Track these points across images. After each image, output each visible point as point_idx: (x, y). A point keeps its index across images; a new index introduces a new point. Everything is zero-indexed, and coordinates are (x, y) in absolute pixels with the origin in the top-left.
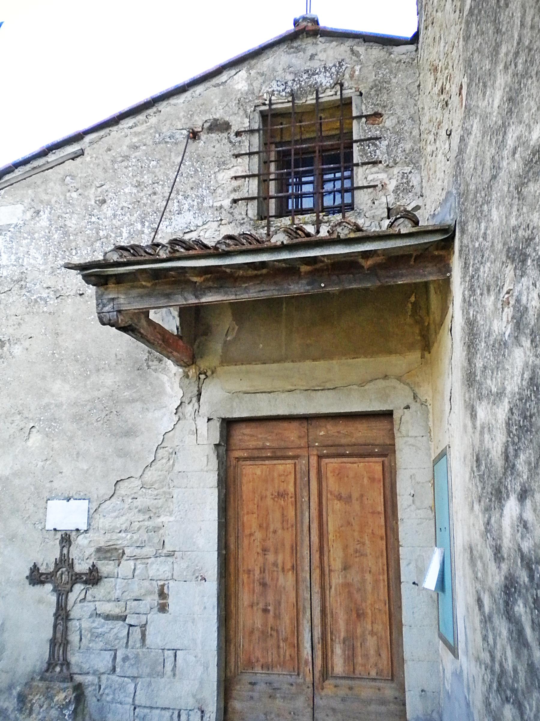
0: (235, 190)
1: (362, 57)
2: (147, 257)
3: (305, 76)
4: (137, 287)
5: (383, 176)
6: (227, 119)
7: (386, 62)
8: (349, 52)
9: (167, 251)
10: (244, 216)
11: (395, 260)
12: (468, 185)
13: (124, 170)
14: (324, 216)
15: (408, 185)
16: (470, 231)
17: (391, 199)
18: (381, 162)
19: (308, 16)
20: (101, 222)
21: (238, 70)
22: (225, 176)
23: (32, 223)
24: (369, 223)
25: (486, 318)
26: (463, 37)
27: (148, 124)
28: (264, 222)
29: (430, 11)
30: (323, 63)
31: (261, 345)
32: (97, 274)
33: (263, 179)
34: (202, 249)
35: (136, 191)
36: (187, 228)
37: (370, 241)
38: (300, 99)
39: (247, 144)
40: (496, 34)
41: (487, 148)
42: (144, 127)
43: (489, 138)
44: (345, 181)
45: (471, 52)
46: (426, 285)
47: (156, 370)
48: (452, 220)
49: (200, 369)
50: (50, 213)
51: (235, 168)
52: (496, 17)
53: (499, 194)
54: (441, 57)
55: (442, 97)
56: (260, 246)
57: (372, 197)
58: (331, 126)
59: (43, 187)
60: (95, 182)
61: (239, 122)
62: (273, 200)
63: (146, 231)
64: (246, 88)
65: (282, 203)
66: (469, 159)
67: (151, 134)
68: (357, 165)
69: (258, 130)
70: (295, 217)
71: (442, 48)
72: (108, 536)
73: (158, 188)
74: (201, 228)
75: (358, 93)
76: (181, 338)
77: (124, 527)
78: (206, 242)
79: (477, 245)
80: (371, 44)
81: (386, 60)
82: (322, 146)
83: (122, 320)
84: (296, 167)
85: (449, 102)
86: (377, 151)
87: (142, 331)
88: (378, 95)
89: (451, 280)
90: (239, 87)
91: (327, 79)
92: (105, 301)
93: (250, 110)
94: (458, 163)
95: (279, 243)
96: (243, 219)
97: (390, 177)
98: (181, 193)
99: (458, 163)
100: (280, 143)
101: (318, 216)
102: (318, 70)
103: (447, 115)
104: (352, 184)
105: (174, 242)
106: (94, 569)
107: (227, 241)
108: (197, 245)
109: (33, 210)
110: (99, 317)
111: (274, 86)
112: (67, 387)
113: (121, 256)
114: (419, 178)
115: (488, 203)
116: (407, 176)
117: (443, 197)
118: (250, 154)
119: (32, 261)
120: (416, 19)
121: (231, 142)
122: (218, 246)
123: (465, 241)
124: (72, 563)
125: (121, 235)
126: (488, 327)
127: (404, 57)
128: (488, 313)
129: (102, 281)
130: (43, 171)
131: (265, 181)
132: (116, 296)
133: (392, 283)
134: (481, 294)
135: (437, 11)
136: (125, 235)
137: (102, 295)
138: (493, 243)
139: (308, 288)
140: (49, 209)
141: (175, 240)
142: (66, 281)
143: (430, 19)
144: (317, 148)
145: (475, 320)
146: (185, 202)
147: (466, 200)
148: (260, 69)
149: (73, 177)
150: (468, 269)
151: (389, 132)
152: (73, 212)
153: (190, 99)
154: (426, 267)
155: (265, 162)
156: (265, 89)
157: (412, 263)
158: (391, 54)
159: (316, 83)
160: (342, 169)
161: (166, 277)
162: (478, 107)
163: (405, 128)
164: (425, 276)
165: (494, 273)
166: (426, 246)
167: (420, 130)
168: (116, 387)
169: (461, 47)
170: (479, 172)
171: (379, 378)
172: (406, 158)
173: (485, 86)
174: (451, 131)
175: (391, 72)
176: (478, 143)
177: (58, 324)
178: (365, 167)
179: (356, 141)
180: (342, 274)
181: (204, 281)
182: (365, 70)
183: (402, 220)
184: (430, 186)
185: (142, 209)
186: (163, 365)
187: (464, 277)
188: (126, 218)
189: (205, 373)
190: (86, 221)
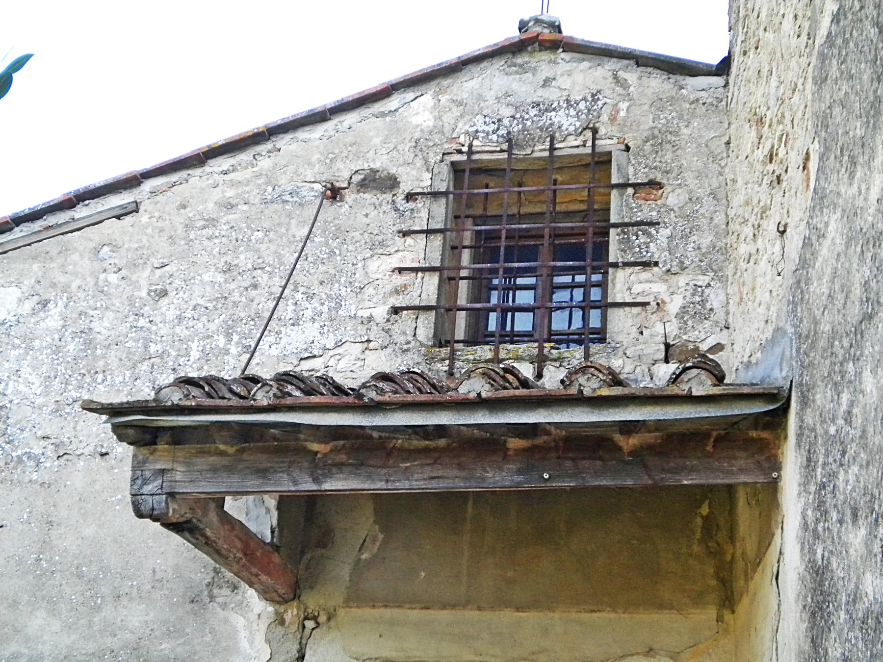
0: (397, 292)
1: (632, 89)
2: (235, 401)
3: (533, 112)
4: (209, 453)
5: (659, 288)
6: (393, 171)
7: (672, 100)
8: (611, 80)
9: (271, 394)
10: (410, 338)
11: (680, 441)
12: (816, 323)
13: (206, 242)
14: (552, 348)
15: (704, 307)
16: (818, 402)
17: (673, 328)
18: (656, 264)
19: (544, 17)
20: (154, 328)
21: (419, 94)
22: (380, 267)
23: (33, 320)
24: (632, 367)
25: (849, 566)
26: (814, 78)
27: (254, 169)
28: (445, 351)
29: (753, 28)
30: (565, 93)
31: (423, 574)
32: (141, 426)
33: (448, 277)
34: (334, 394)
35: (222, 280)
36: (306, 350)
37: (636, 404)
38: (521, 147)
39: (424, 214)
40: (875, 84)
41: (855, 265)
42: (248, 173)
43: (859, 249)
44: (593, 290)
45: (828, 104)
46: (730, 489)
47: (224, 606)
48: (785, 378)
49: (306, 608)
50: (66, 306)
51: (400, 253)
52: (876, 56)
53: (877, 348)
54: (772, 103)
55: (771, 168)
56: (437, 397)
57: (638, 321)
58: (573, 195)
59: (60, 260)
60: (152, 260)
61: (414, 177)
62: (462, 315)
63: (233, 350)
64: (431, 124)
65: (478, 317)
66: (820, 279)
67: (259, 185)
68: (615, 265)
69: (446, 194)
70: (501, 346)
71: (773, 91)
73: (262, 278)
74: (331, 353)
75: (623, 147)
76: (277, 548)
78: (338, 379)
79: (832, 430)
80: (649, 69)
81: (673, 97)
82: (555, 228)
83: (174, 510)
84: (506, 261)
85: (784, 177)
86: (651, 244)
87: (208, 532)
88: (657, 152)
89: (781, 484)
90: (415, 120)
91: (571, 120)
92: (147, 474)
93: (434, 158)
94: (799, 282)
95: (473, 395)
96: (408, 343)
97: (671, 290)
98: (302, 289)
99: (799, 282)
100: (481, 217)
101: (541, 348)
102: (555, 104)
103: (778, 198)
104: (605, 294)
105: (284, 378)
107: (380, 385)
108: (325, 385)
109: (36, 299)
110: (133, 503)
111: (479, 124)
112: (56, 625)
113: (187, 396)
114: (722, 297)
115: (856, 359)
116: (703, 292)
117: (768, 334)
118: (428, 232)
119: (22, 388)
120: (726, 37)
121: (396, 210)
122: (363, 391)
123: (809, 420)
125: (188, 354)
126: (853, 585)
127: (703, 94)
128: (853, 558)
129: (148, 437)
130: (62, 234)
131: (450, 279)
132: (167, 466)
133: (671, 482)
134: (841, 522)
135: (765, 30)
136: (195, 354)
137: (145, 462)
138: (864, 431)
139: (518, 478)
140: (65, 300)
141: (286, 374)
142: (78, 428)
143: (753, 41)
144: (547, 231)
145: (827, 567)
146: (309, 306)
147: (813, 346)
148: (457, 95)
149: (115, 248)
150: (814, 470)
151: (673, 215)
152: (107, 308)
153: (332, 133)
154: (734, 458)
155: (454, 248)
156: (462, 127)
157: (709, 448)
158: (681, 88)
159: (552, 124)
160: (589, 270)
161: (262, 438)
162: (839, 194)
163: (702, 211)
164: (733, 473)
165: (865, 487)
166: (735, 420)
167: (727, 216)
168: (148, 631)
169: (808, 92)
170: (839, 304)
171: (637, 653)
172: (701, 261)
173: (853, 161)
174: (786, 226)
175: (681, 117)
176: (839, 255)
177: (54, 506)
178: (629, 270)
179: (616, 226)
180: (584, 459)
181: (331, 451)
182: (636, 111)
183: (695, 371)
184: (743, 313)
185: (231, 312)
186: (239, 597)
187: (805, 485)
188: (200, 325)
189: (315, 618)
190: (128, 325)
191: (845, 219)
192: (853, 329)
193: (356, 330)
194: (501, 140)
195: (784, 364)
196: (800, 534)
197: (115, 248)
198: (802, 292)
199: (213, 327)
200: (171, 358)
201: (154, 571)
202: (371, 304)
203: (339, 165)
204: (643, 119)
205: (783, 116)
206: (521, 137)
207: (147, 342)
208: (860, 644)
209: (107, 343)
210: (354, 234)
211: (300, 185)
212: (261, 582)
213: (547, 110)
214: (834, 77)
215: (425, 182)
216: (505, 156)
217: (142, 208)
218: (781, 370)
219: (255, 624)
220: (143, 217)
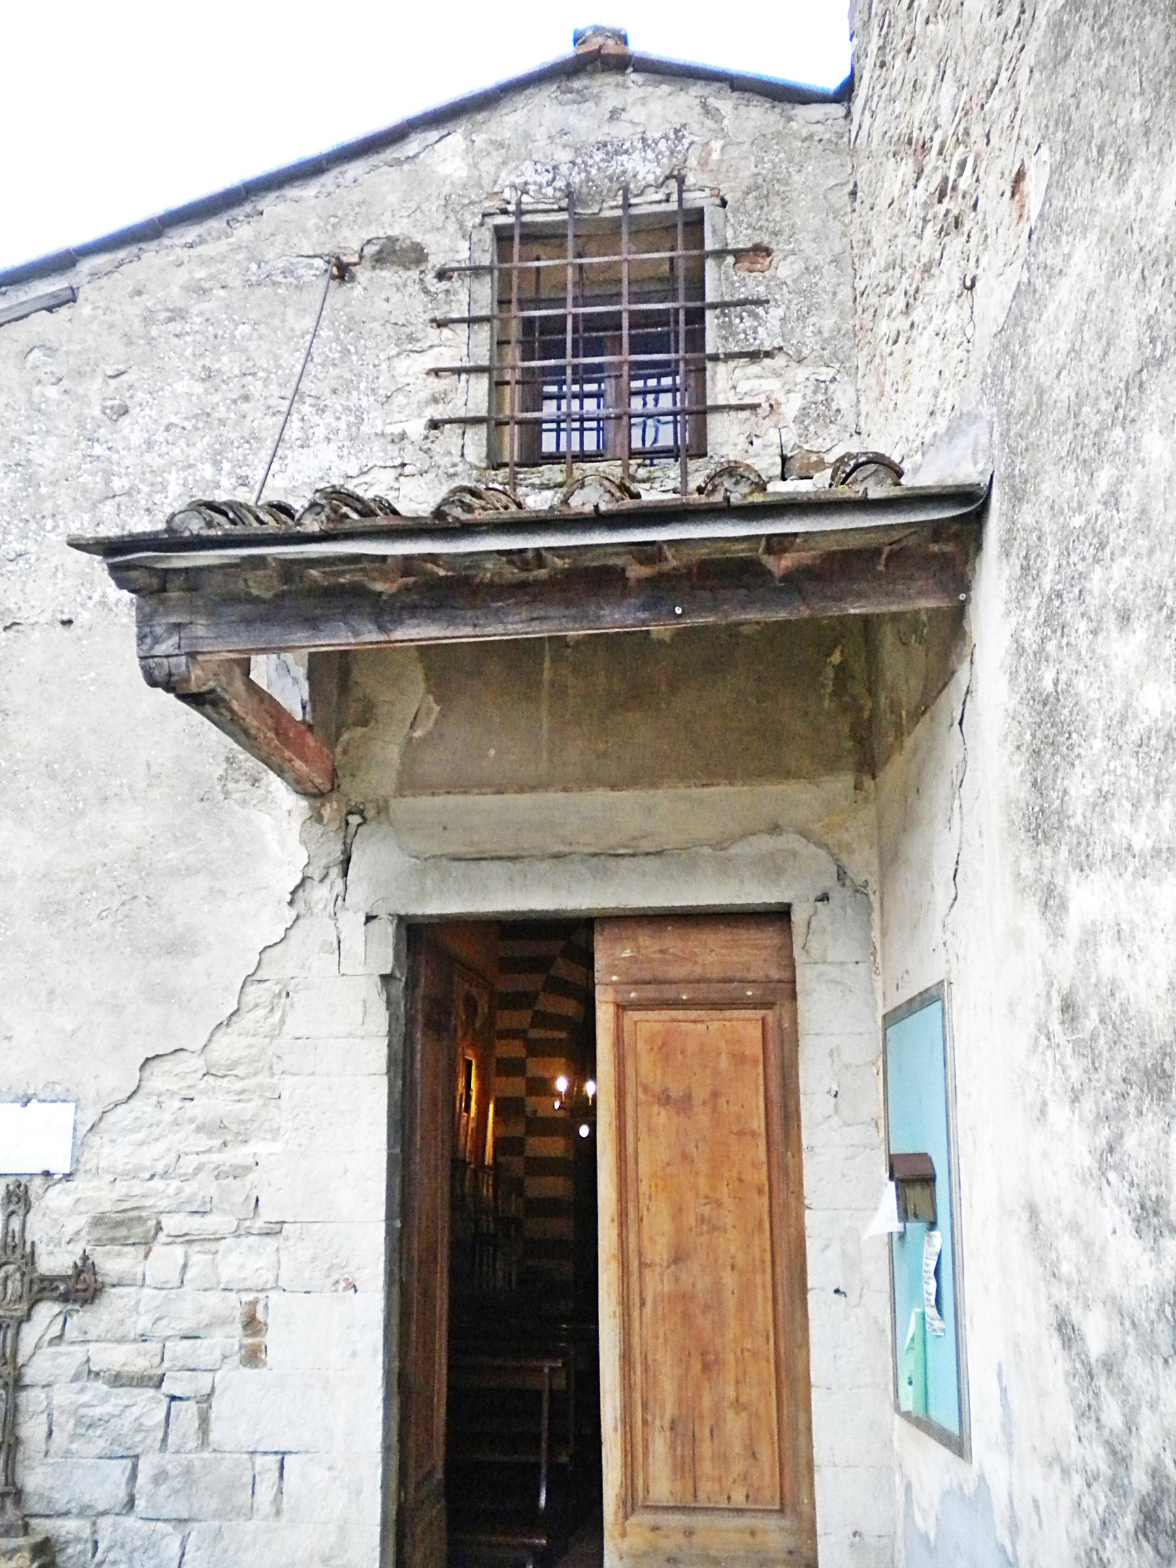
0: (435, 400)
1: (726, 122)
3: (599, 156)
5: (772, 385)
8: (698, 109)
9: (323, 517)
10: (458, 459)
13: (175, 341)
14: (639, 466)
15: (828, 408)
20: (115, 457)
21: (445, 132)
22: (413, 367)
30: (640, 129)
35: (201, 391)
36: (322, 479)
38: (585, 204)
39: (464, 297)
42: (222, 246)
45: (1070, 92)
47: (244, 803)
48: (981, 473)
51: (436, 350)
57: (747, 429)
60: (103, 365)
64: (464, 174)
68: (715, 358)
69: (490, 270)
70: (575, 466)
72: (122, 1188)
73: (255, 387)
75: (718, 201)
76: (310, 727)
77: (160, 1167)
80: (747, 95)
81: (779, 133)
87: (235, 705)
88: (762, 208)
91: (649, 166)
93: (471, 221)
94: (1006, 347)
95: (589, 508)
96: (454, 465)
97: (787, 387)
101: (626, 467)
106: (85, 1268)
110: (143, 668)
111: (528, 174)
114: (851, 394)
116: (827, 389)
118: (471, 321)
121: (426, 292)
124: (33, 1253)
127: (819, 127)
142: (28, 590)
149: (50, 351)
152: (48, 432)
154: (911, 578)
158: (790, 119)
159: (624, 172)
162: (1093, 211)
163: (822, 283)
168: (148, 838)
171: (760, 831)
178: (732, 364)
179: (713, 306)
181: (399, 591)
182: (734, 152)
183: (873, 467)
185: (216, 432)
186: (261, 791)
189: (361, 813)
190: (79, 453)
191: (1108, 241)
192: (1122, 385)
193: (386, 452)
194: (558, 194)
195: (980, 456)
196: (1008, 661)
197: (50, 351)
198: (1013, 357)
199: (194, 453)
200: (143, 495)
201: (148, 765)
202: (402, 417)
203: (345, 232)
204: (743, 163)
205: (967, 133)
206: (585, 190)
207: (108, 475)
208: (1133, 772)
209: (54, 478)
210: (372, 325)
211: (294, 260)
212: (294, 770)
213: (617, 153)
214: (1084, 50)
215: (462, 254)
216: (564, 216)
217: (81, 297)
218: (975, 463)
219: (285, 824)
220: (83, 309)
